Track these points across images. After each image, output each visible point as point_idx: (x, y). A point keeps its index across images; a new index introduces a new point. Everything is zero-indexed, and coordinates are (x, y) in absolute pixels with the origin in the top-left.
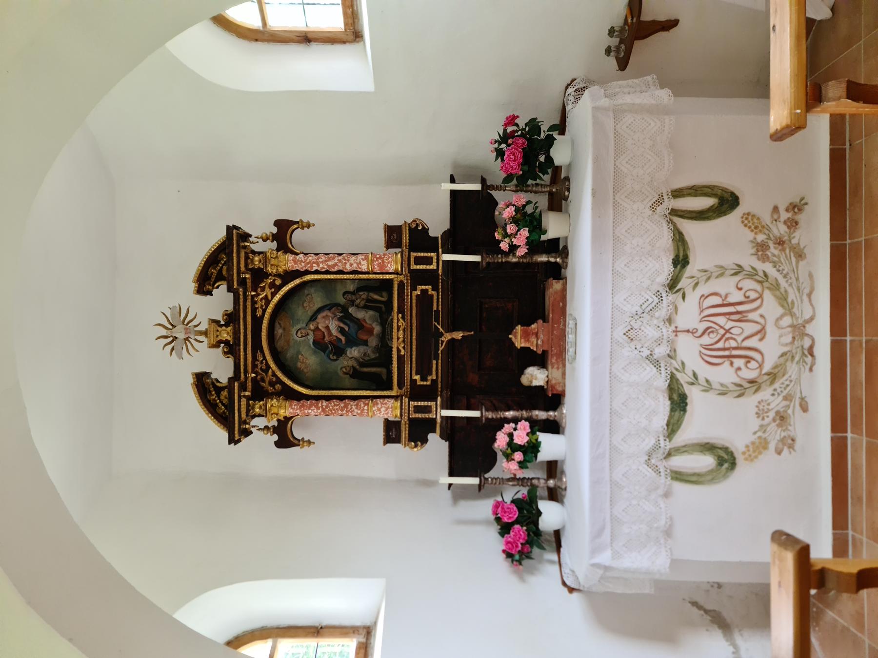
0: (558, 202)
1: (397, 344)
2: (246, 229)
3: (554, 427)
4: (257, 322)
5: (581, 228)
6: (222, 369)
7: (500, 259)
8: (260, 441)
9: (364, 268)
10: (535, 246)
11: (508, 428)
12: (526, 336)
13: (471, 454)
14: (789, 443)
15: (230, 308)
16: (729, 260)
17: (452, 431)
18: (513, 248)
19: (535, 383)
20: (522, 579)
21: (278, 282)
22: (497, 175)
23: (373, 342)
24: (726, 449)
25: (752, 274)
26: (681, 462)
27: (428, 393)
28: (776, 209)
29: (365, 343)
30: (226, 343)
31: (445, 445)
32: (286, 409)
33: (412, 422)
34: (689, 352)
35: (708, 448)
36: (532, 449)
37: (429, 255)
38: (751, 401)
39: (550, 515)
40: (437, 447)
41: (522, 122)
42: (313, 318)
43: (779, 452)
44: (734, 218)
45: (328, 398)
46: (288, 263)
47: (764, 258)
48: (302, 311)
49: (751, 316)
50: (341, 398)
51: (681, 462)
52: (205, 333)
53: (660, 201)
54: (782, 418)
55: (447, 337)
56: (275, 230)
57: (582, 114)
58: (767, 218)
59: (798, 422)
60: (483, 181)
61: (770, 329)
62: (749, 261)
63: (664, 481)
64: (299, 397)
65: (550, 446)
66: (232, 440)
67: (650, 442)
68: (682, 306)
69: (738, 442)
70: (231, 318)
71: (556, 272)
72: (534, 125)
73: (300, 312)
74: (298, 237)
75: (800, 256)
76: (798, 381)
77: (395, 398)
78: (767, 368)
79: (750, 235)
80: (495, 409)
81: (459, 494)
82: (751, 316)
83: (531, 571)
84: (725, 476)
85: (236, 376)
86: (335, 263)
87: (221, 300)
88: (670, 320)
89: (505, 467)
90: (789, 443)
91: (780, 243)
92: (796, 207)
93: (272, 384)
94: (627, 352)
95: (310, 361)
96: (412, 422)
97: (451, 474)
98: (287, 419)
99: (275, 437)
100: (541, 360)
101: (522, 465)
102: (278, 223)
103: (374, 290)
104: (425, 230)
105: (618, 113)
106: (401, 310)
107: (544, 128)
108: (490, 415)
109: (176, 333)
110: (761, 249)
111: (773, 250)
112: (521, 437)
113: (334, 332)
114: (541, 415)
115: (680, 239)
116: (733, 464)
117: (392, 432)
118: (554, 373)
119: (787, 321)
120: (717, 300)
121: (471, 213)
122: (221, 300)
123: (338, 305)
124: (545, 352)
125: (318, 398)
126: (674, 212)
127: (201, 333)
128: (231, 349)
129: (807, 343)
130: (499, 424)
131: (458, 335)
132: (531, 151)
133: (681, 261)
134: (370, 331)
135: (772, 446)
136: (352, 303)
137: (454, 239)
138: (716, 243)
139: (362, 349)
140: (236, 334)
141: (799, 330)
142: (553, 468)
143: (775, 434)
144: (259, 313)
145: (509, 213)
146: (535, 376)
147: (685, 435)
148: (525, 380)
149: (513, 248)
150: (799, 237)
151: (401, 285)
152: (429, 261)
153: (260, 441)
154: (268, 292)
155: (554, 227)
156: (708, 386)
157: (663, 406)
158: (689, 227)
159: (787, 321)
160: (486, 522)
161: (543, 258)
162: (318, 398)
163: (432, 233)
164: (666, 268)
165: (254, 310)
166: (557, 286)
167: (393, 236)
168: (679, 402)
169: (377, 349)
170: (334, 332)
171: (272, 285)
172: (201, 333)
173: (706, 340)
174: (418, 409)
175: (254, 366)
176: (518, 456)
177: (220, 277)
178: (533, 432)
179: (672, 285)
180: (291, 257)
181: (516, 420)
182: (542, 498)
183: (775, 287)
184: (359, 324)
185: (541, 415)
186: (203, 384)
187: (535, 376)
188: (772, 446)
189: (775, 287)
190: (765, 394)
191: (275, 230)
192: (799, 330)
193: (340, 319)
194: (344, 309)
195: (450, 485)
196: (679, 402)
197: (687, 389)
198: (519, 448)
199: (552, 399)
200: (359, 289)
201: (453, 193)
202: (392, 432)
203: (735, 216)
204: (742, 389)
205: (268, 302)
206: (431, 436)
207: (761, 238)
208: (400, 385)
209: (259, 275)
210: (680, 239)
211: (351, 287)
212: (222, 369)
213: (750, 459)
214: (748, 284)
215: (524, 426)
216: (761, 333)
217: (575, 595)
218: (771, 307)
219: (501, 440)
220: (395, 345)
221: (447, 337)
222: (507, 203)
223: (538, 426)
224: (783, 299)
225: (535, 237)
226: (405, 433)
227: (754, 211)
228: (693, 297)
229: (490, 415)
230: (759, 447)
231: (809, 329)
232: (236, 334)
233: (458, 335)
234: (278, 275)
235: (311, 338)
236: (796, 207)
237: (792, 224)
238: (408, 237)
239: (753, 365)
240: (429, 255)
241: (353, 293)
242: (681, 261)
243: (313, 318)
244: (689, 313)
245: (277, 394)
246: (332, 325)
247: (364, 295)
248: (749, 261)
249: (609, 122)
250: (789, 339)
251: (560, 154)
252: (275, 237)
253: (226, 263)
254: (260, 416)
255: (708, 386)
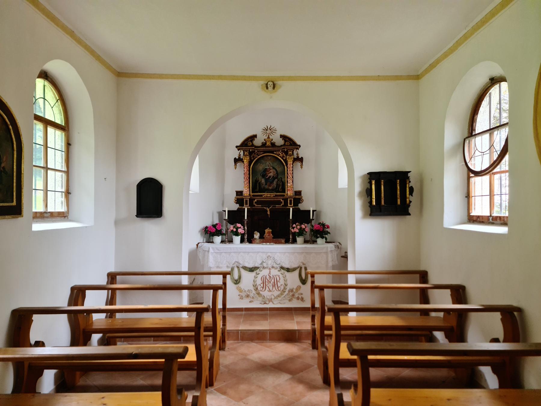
0: (306, 242)
1: (266, 194)
2: (300, 149)
3: (242, 241)
4: (272, 152)
5: (299, 246)
6: (258, 142)
7: (291, 225)
8: (236, 153)
9: (288, 185)
10: (294, 234)
11: (242, 227)
12: (269, 233)
13: (234, 217)
14: (241, 298)
15: (277, 144)
16: (289, 283)
17: (240, 212)
18: (293, 228)
19: (255, 235)
20: (199, 231)
21: (284, 158)
22: (313, 223)
23: (266, 187)
24: (239, 282)
25: (285, 288)
26: (236, 270)
27: (251, 204)
28: (302, 294)
29: (266, 184)
30: (266, 143)
31: (236, 209)
32: (246, 161)
33: (243, 199)
34: (265, 272)
35: (240, 277)
36: (237, 234)
37: (15, 201)
38: (252, 288)
39: (218, 239)
40: (235, 207)
41: (328, 230)
42: (274, 168)
43: (239, 295)
44: (299, 283)
45: (249, 174)
46: (290, 162)
47: (289, 291)
48: (276, 165)
49: (274, 288)
50: (249, 178)
51: (236, 270)
52: (269, 138)
53: (304, 264)
54: (248, 296)
55: (268, 210)
56: (300, 157)
57: (331, 246)
58: (300, 292)
59: (247, 300)
60: (313, 219)
61: (271, 293)
62: (288, 288)
63: (231, 265)
64: (250, 165)
65: (237, 239)
66: (237, 147)
67: (241, 263)
68: (276, 271)
69: (242, 285)
70: (273, 145)
71: (287, 242)
72: (328, 233)
73: (275, 164)
74: (299, 164)
75: (290, 300)
76: (258, 300)
77: (250, 194)
78: (261, 292)
79: (295, 288)
80: (247, 224)
81: (220, 214)
82: (274, 288)
83: (201, 234)
84: (233, 282)
85: (256, 147)
86: (290, 176)
87: (279, 142)
88: (273, 267)
89: (231, 227)
90: (241, 298)
91: (293, 295)
92: (302, 299)
93: (253, 157)
94: (265, 256)
95: (261, 167)
96: (243, 199)
97: (228, 211)
98: (243, 162)
99: (237, 158)
100: (262, 237)
101: (232, 231)
102: (302, 158)
103: (282, 187)
104: (300, 203)
105: (326, 253)
106: (276, 195)
107: (326, 236)
108: (246, 222)
109: (268, 130)
110: (291, 290)
111: (291, 294)
112: (241, 231)
113: (269, 175)
114: (246, 237)
115: (294, 270)
116: (236, 284)
117: (239, 193)
118: (258, 241)
119: (273, 297)
120: (278, 279)
121: (303, 216)
122: (279, 142)
123: (278, 176)
124: (264, 238)
125: (249, 171)
126: (301, 268)
127: (269, 136)
128: (264, 145)
129: (267, 302)
130: (243, 225)
131: (269, 213)
132: (320, 232)
133: (288, 270)
134: (270, 186)
135: (241, 294)
136: (278, 180)
137: (297, 212)
138: (293, 279)
139: (264, 183)
140: (269, 147)
141: (270, 300)
142: (231, 241)
143: (244, 294)
144: (275, 153)
145: (303, 226)
146: (257, 235)
147: (243, 271)
148: (256, 232)
149: (293, 228)
150: (295, 300)
151: (284, 196)
152: (291, 204)
153: (236, 153)
154: (281, 155)
155: (300, 239)
156: (256, 277)
157: (250, 265)
158: (297, 272)
159: (273, 297)
160: (213, 222)
161: (291, 237)
162: (249, 171)
163: (299, 205)
164: (286, 266)
165: (276, 151)
166: (283, 241)
167: (298, 193)
168: (251, 270)
169: (264, 188)
170: (269, 175)
171: (283, 156)
172: (269, 136)
173: (268, 277)
174: (246, 201)
175: (259, 151)
176: (235, 230)
177: (285, 141)
178: (241, 234)
179: (282, 268)
180: (291, 163)
181: (244, 229)
182: (222, 238)
183: (282, 294)
184: (272, 182)
185: (246, 237)
186: (254, 137)
187: (257, 235)
188: (241, 294)
189: (282, 294)
190: (254, 292)
191: (300, 157)
192: (270, 300)
193: (273, 176)
194: (276, 178)
195: (225, 211)
196: (251, 270)
197: (255, 272)
198: (237, 230)
199: (251, 240)
200: (283, 182)
201: (310, 211)
202: (239, 193)
203: (300, 284)
204: (255, 286)
205: (278, 155)
206: (238, 205)
207: (294, 290)
208: (253, 195)
209: (286, 153)
210: (294, 270)
211: (283, 180)
212: (258, 142)
213: (237, 288)
214: (282, 287)
215: (243, 232)
216: (270, 291)
217: (196, 246)
218: (276, 293)
219: (239, 225)
220: (266, 194)
221: (268, 210)
222: (307, 227)
223: (243, 236)
224: (278, 296)
225: (297, 234)
226: (239, 197)
227: (301, 288)
228: (279, 273)
229: (246, 222)
230: (240, 290)
231: (271, 303)
232: (269, 147)
233: (269, 213)
234: (286, 159)
235: (267, 167)
236: (302, 299)
237: (298, 298)
238: (298, 197)
239: (261, 289)
240: (15, 201)
241: (281, 180)
242: (288, 270)
243: (274, 168)
244: (275, 272)
245: (250, 159)
246: (271, 174)
247: (281, 184)
248: (288, 288)
249: (324, 251)
250: (268, 298)
251: (319, 240)
252: (298, 157)
253: (290, 144)
254: (244, 154)
255: (256, 277)
